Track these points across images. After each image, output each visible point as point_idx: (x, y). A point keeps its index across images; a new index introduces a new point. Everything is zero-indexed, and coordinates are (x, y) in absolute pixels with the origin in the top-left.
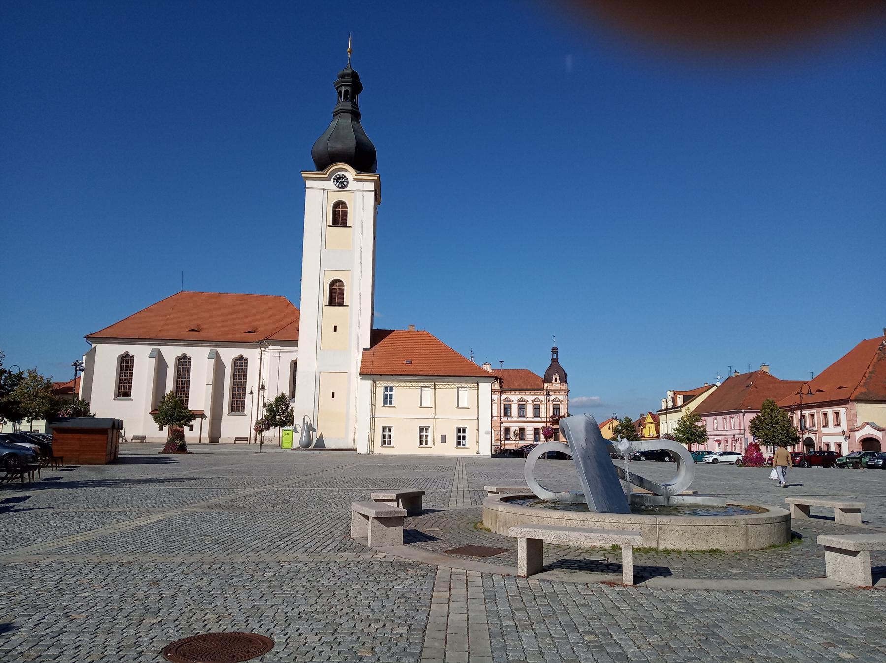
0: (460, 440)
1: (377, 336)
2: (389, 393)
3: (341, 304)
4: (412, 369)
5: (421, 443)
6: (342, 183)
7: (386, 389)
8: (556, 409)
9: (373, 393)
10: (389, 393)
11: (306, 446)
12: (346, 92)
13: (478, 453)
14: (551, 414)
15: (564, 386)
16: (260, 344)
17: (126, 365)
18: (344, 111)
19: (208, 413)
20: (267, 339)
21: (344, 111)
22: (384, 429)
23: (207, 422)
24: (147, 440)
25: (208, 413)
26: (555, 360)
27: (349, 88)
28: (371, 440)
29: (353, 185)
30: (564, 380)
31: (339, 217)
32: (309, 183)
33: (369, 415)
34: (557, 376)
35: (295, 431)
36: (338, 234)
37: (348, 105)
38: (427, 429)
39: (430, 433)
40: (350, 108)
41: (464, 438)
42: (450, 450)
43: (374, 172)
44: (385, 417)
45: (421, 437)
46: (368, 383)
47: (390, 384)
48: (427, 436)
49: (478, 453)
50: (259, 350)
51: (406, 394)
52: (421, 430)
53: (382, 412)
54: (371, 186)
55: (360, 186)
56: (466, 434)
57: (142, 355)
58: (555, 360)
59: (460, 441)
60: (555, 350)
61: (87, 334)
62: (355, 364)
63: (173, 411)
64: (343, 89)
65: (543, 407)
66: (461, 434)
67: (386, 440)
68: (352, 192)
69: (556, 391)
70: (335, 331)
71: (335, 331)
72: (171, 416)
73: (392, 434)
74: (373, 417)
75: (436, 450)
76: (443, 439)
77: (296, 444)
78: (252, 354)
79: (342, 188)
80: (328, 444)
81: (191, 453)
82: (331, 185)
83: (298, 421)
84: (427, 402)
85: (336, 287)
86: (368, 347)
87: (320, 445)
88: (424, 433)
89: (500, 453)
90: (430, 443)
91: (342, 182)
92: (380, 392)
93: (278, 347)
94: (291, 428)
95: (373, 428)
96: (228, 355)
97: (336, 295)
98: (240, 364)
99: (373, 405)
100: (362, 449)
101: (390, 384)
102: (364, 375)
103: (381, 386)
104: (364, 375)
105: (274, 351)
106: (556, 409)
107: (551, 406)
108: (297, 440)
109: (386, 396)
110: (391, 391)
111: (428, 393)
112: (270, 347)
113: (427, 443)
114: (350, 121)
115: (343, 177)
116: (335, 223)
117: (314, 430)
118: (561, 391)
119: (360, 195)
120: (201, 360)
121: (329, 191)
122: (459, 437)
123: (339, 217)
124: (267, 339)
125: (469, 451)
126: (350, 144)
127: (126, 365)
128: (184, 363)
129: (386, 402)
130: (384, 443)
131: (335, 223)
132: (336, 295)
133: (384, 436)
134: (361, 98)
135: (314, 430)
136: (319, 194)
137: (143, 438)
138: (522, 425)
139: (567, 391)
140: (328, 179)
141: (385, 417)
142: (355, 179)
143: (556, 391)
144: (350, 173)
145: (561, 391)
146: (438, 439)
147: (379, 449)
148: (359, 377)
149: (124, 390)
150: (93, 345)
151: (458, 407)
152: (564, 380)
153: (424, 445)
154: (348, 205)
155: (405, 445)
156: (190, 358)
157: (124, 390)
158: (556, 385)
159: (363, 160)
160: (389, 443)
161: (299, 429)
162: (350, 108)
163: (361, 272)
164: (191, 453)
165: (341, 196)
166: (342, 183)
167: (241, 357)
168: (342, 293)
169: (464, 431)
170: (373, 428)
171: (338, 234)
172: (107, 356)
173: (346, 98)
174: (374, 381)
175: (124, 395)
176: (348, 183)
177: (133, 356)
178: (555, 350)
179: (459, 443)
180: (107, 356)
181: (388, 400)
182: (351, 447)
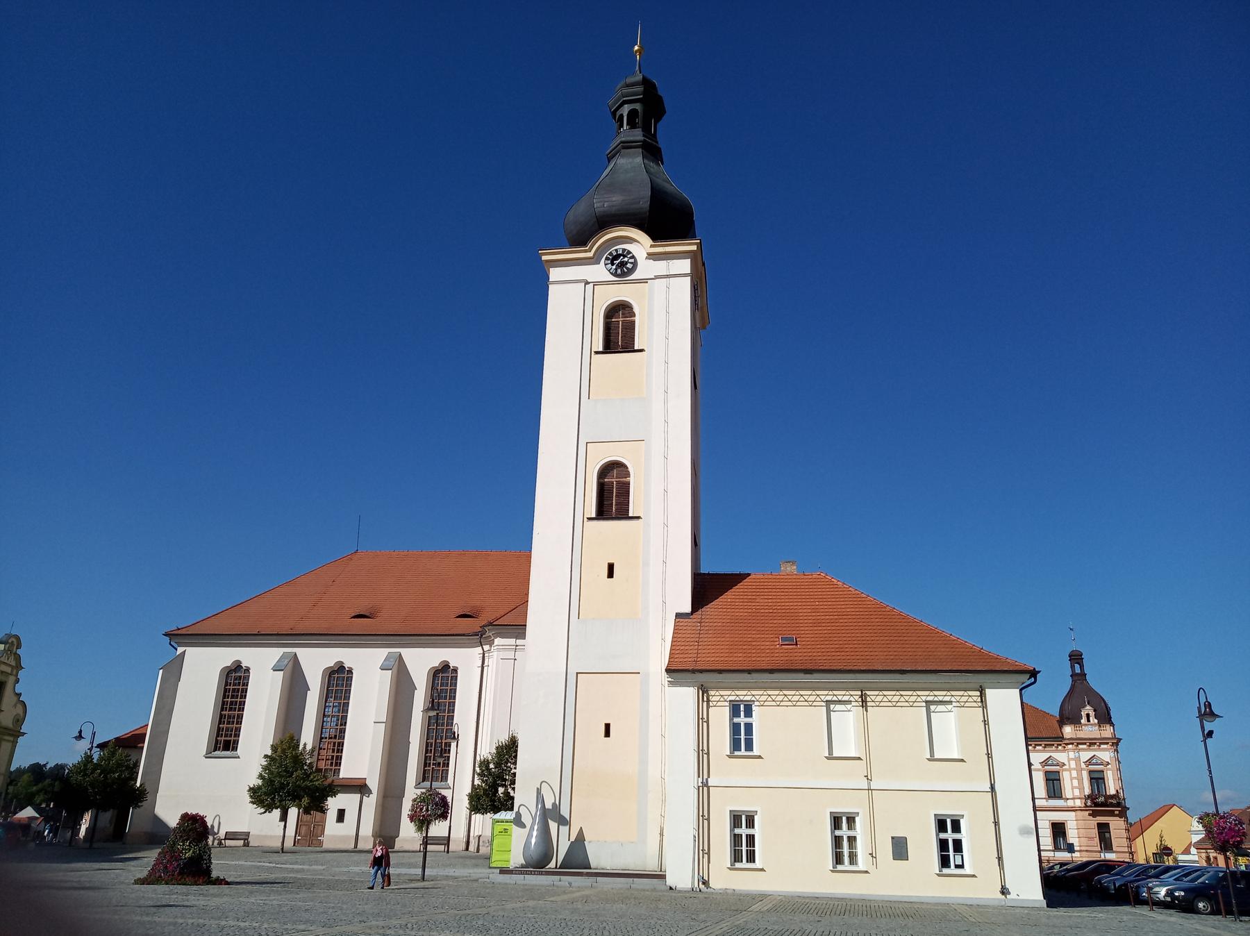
0: (948, 852)
1: (707, 588)
2: (742, 720)
3: (623, 514)
4: (798, 655)
5: (838, 859)
6: (622, 266)
7: (735, 709)
8: (1097, 779)
9: (703, 721)
10: (742, 720)
11: (538, 863)
12: (632, 114)
13: (1004, 891)
14: (1087, 791)
15: (1107, 732)
16: (480, 637)
17: (234, 686)
18: (627, 145)
19: (374, 784)
20: (491, 624)
21: (627, 145)
22: (736, 819)
23: (371, 802)
24: (253, 842)
25: (374, 784)
26: (1079, 678)
27: (638, 106)
28: (703, 851)
29: (646, 268)
30: (1105, 717)
31: (618, 332)
32: (555, 274)
33: (692, 780)
34: (1089, 709)
35: (518, 822)
36: (619, 371)
37: (638, 135)
38: (851, 820)
39: (860, 829)
40: (641, 138)
41: (958, 846)
42: (920, 880)
43: (694, 237)
44: (736, 782)
45: (837, 841)
46: (687, 695)
47: (743, 695)
48: (852, 840)
49: (1004, 891)
50: (479, 650)
51: (789, 720)
52: (836, 821)
53: (729, 772)
54: (685, 266)
55: (661, 267)
56: (964, 835)
57: (262, 663)
58: (1079, 678)
59: (948, 852)
60: (1076, 658)
61: (171, 628)
62: (657, 649)
63: (297, 782)
64: (625, 110)
65: (1066, 777)
66: (950, 836)
67: (743, 850)
68: (644, 281)
69: (1092, 743)
70: (611, 575)
71: (611, 575)
72: (282, 786)
73: (757, 832)
74: (705, 784)
75: (879, 880)
76: (900, 848)
77: (516, 858)
78: (464, 659)
79: (624, 274)
80: (599, 857)
81: (219, 881)
82: (600, 271)
83: (523, 795)
84: (847, 744)
85: (612, 479)
86: (688, 609)
87: (577, 861)
88: (844, 832)
89: (1067, 886)
90: (863, 862)
91: (623, 264)
92: (720, 718)
93: (512, 641)
94: (509, 815)
95: (704, 817)
96: (421, 661)
97: (612, 496)
98: (444, 677)
99: (703, 753)
100: (680, 876)
101: (743, 695)
102: (676, 672)
103: (721, 699)
104: (676, 672)
105: (504, 648)
106: (1097, 779)
107: (1085, 775)
108: (515, 845)
109: (735, 728)
110: (749, 713)
111: (848, 720)
112: (498, 641)
113: (853, 858)
114: (639, 160)
115: (626, 253)
116: (610, 346)
117: (563, 821)
118: (1103, 741)
119: (663, 289)
120: (369, 668)
121: (596, 284)
122: (943, 845)
123: (618, 332)
124: (491, 624)
125: (975, 884)
126: (642, 198)
127: (234, 686)
128: (339, 679)
129: (736, 745)
130: (737, 857)
131: (610, 346)
132: (612, 496)
133: (736, 839)
134: (664, 131)
135: (563, 821)
136: (574, 294)
137: (245, 837)
138: (1058, 817)
139: (1116, 743)
140: (594, 260)
141: (736, 782)
142: (651, 256)
143: (1092, 743)
144: (640, 244)
145: (1103, 741)
146: (886, 849)
147: (724, 877)
148: (665, 678)
149: (225, 738)
150: (180, 650)
151: (932, 759)
152: (1105, 717)
153: (846, 866)
154: (636, 310)
155: (793, 865)
156: (350, 671)
157: (225, 738)
158: (1090, 729)
159: (666, 220)
160: (751, 857)
161: (526, 819)
162: (641, 138)
163: (666, 440)
164: (219, 881)
165: (621, 292)
166: (622, 266)
167: (445, 667)
168: (624, 490)
169: (956, 827)
170: (704, 817)
171: (619, 371)
172: (203, 668)
173: (632, 124)
174: (704, 690)
175: (226, 748)
176: (635, 264)
177: (248, 670)
178: (1076, 658)
179: (945, 862)
180: (203, 668)
181: (741, 739)
182: (651, 866)
